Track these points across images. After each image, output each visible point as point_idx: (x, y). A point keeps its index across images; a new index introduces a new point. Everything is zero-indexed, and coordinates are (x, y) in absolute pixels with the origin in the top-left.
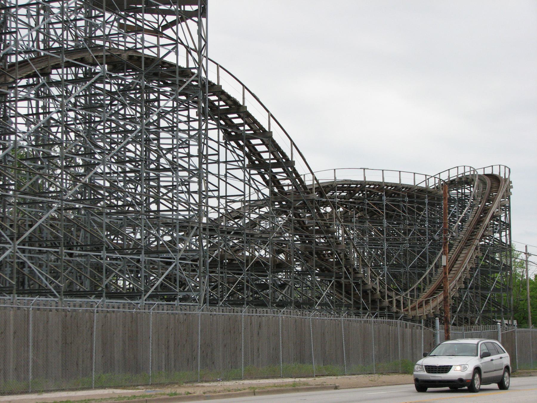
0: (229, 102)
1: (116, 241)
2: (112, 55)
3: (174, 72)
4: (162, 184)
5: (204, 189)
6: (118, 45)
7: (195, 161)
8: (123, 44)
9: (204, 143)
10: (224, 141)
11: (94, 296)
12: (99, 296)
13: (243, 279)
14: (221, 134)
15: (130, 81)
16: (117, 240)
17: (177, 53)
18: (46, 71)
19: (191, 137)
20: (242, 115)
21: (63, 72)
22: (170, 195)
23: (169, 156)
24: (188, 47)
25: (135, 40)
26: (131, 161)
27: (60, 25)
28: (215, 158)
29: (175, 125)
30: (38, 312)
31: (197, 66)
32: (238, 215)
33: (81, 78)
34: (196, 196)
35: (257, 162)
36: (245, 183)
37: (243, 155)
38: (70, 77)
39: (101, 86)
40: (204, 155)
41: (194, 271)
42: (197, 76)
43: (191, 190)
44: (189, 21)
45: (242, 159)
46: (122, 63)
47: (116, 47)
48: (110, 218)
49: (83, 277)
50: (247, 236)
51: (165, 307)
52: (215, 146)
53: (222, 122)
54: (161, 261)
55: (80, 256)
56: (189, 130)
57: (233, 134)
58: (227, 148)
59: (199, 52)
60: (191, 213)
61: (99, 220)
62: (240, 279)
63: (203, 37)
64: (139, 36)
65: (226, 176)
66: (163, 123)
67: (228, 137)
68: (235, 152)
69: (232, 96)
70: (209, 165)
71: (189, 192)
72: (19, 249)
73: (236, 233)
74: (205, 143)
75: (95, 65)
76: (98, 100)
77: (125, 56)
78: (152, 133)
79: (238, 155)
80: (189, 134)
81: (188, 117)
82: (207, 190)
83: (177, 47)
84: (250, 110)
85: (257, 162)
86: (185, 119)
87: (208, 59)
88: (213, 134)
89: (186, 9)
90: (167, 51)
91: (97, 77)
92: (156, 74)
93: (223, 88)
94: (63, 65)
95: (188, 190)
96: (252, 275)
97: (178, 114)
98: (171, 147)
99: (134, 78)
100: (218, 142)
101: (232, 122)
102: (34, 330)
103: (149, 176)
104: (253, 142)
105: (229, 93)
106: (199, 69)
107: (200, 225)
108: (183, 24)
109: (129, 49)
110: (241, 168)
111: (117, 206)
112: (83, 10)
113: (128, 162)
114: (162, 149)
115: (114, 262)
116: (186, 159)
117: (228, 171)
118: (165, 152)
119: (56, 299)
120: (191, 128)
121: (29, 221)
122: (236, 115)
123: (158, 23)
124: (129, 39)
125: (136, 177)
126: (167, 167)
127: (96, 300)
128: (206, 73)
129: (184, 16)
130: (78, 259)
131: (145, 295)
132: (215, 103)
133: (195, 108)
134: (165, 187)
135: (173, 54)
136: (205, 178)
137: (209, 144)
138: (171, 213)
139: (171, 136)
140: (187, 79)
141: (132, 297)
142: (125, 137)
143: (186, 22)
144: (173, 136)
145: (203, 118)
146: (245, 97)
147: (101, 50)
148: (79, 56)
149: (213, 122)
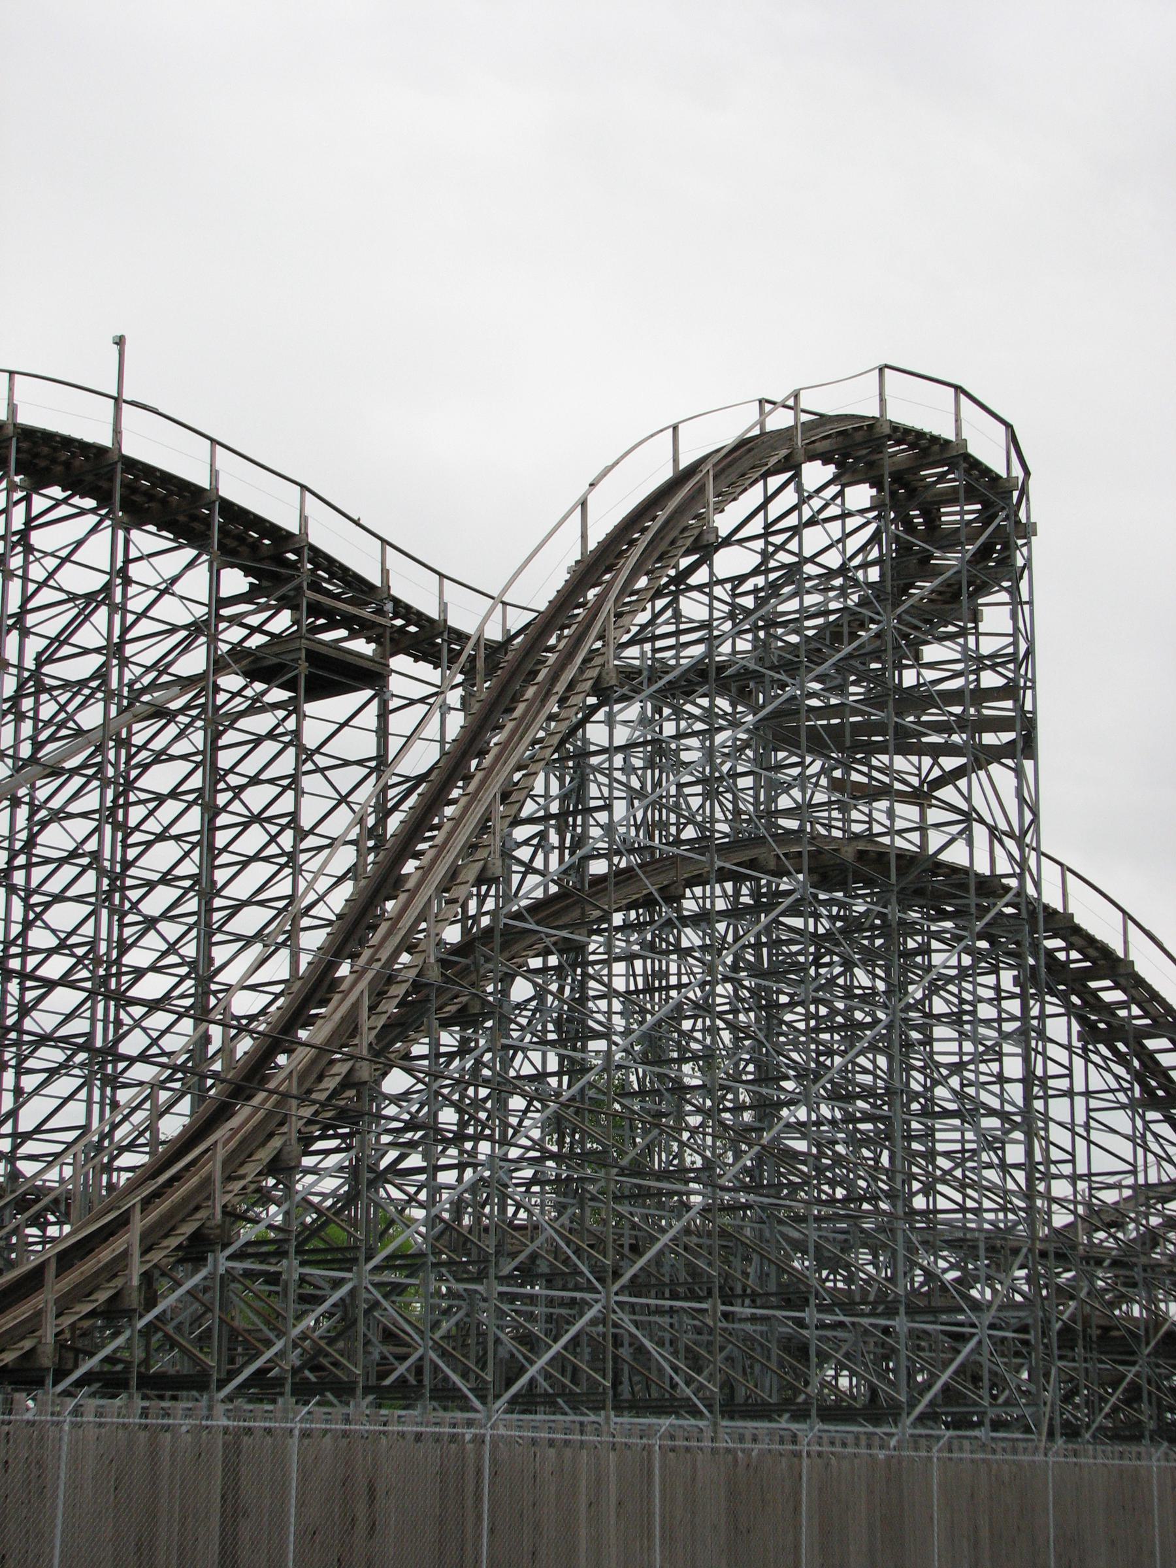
0: (1091, 952)
1: (830, 1284)
2: (820, 852)
3: (964, 887)
4: (940, 1147)
5: (1038, 1157)
6: (829, 827)
7: (1016, 1092)
8: (840, 824)
9: (1036, 1051)
10: (1079, 1045)
11: (786, 1416)
12: (800, 1415)
13: (1137, 1375)
14: (1076, 1027)
15: (862, 909)
16: (835, 1281)
17: (970, 843)
18: (672, 890)
19: (1005, 1036)
20: (1122, 981)
21: (713, 892)
22: (958, 1173)
23: (955, 1082)
24: (996, 828)
25: (870, 815)
26: (868, 1093)
27: (698, 789)
28: (1064, 1084)
29: (967, 1007)
30: (671, 1455)
31: (1018, 870)
32: (1113, 1219)
33: (747, 906)
34: (1020, 1176)
35: (1160, 1093)
36: (1135, 1144)
37: (1128, 1077)
38: (721, 905)
39: (798, 922)
40: (1039, 1079)
41: (1017, 1354)
42: (1018, 895)
43: (1009, 1160)
44: (994, 768)
45: (1126, 1085)
46: (842, 867)
47: (823, 832)
48: (819, 1229)
49: (757, 1367)
50: (1145, 1270)
51: (923, 1442)
52: (1062, 1055)
53: (1075, 1000)
54: (943, 1332)
55: (753, 1319)
56: (1000, 1020)
57: (1102, 1026)
58: (1088, 1060)
59: (1020, 841)
60: (1011, 1216)
61: (796, 1235)
62: (1130, 1376)
63: (1029, 804)
64: (883, 804)
65: (1087, 1127)
66: (939, 1006)
67: (1090, 1034)
68: (1109, 1070)
69: (1098, 937)
70: (1050, 1101)
71: (1004, 1167)
72: (616, 1302)
73: (1116, 1263)
74: (1040, 1049)
75: (780, 873)
76: (784, 954)
77: (848, 853)
78: (915, 1028)
79: (1117, 1077)
80: (999, 1030)
81: (997, 988)
82: (1048, 1161)
83: (969, 829)
84: (1141, 969)
85: (1160, 1093)
86: (991, 994)
87: (1041, 854)
88: (1057, 1028)
89: (984, 742)
90: (948, 838)
91: (789, 901)
92: (919, 892)
93: (1076, 921)
94: (713, 876)
95: (1002, 1160)
96: (1101, 1362)
97: (975, 984)
98: (956, 1059)
99: (872, 903)
100: (1069, 1048)
101: (1100, 999)
102: (663, 1499)
103: (909, 1129)
104: (1151, 1044)
105: (1091, 932)
106: (1021, 877)
107: (1033, 1244)
108: (982, 773)
109: (857, 837)
110: (1123, 1107)
111: (832, 1201)
112: (750, 753)
113: (859, 1096)
114: (938, 1065)
115: (829, 1333)
116: (996, 1088)
117: (1092, 1114)
118: (945, 1072)
119: (701, 1424)
120: (1004, 1015)
121: (631, 1237)
122: (1108, 983)
123: (919, 775)
124: (855, 815)
125: (877, 1131)
126: (953, 1106)
127: (794, 1426)
128: (1037, 885)
129: (983, 758)
130: (749, 1327)
131: (909, 1414)
132: (1058, 954)
133: (1011, 967)
134: (947, 1154)
135: (960, 846)
136: (1042, 1133)
137: (1049, 1054)
138: (960, 1216)
139: (956, 1035)
140: (992, 900)
141: (876, 1420)
142: (850, 1041)
143: (987, 771)
144: (961, 1033)
145: (1032, 991)
146: (1130, 938)
147: (798, 841)
148: (745, 856)
149: (1054, 1000)
